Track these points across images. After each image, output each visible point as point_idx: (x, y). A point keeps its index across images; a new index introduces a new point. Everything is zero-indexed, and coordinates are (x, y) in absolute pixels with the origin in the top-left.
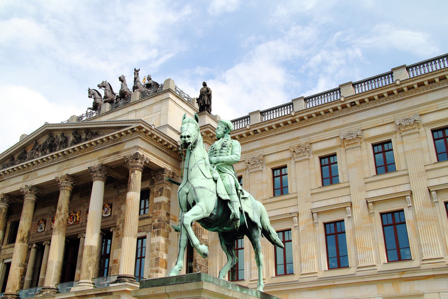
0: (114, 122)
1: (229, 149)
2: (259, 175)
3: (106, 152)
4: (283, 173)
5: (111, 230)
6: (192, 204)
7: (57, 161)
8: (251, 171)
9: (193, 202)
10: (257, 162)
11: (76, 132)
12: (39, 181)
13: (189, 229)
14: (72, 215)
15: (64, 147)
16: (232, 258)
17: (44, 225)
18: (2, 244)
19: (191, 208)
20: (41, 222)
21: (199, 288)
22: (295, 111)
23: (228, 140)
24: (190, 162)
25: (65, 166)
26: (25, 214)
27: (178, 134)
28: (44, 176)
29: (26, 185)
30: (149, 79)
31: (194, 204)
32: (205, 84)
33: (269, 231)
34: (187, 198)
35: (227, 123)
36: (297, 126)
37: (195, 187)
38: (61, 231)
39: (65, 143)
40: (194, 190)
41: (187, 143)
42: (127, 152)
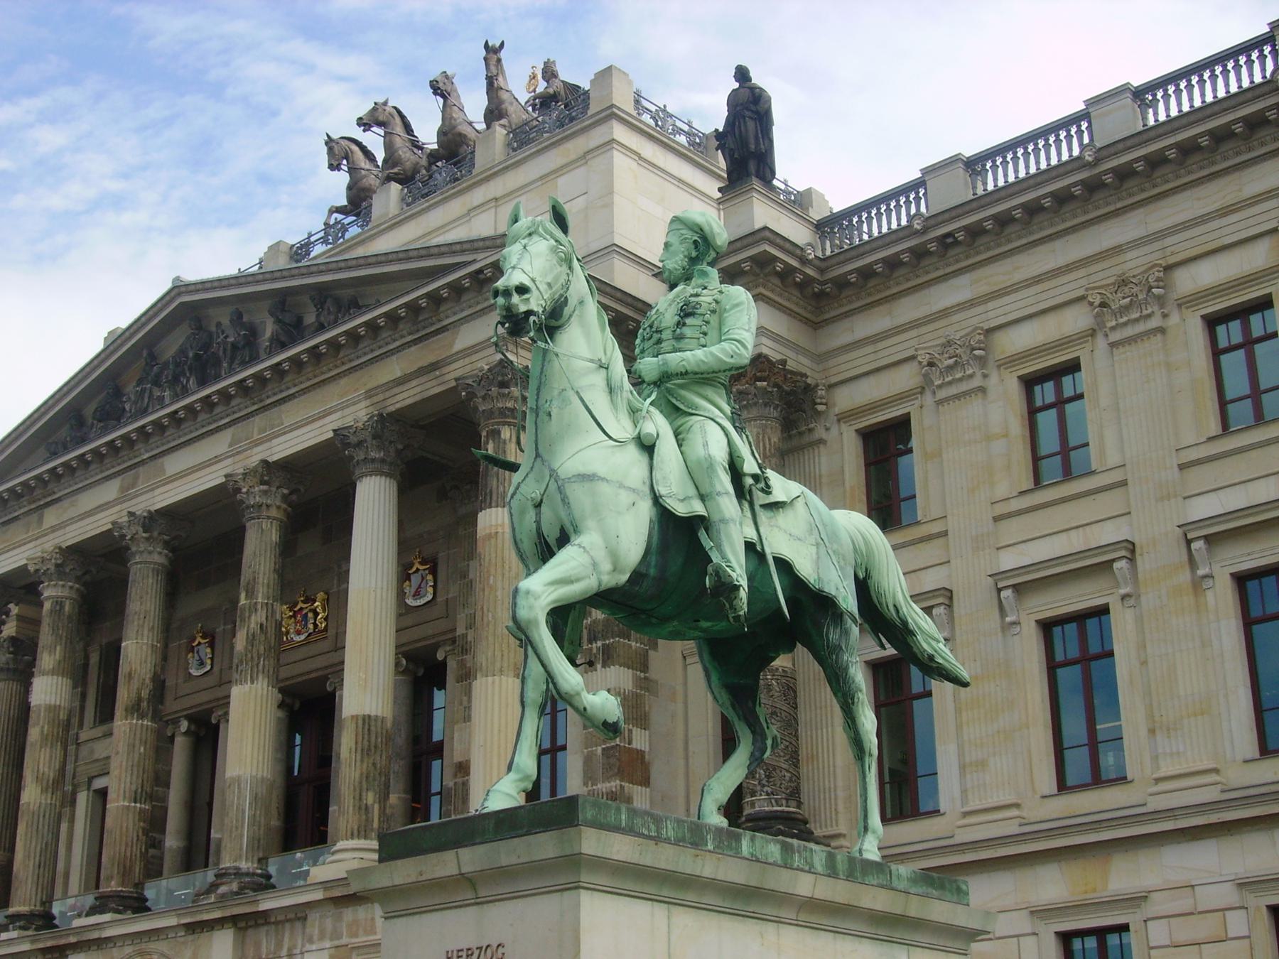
0: (427, 252)
1: (708, 322)
2: (972, 410)
3: (393, 369)
4: (1068, 392)
5: (440, 656)
7: (228, 415)
8: (942, 394)
9: (559, 535)
10: (965, 358)
11: (283, 303)
12: (172, 493)
13: (540, 636)
15: (245, 364)
17: (209, 650)
18: (81, 725)
20: (199, 639)
21: (568, 853)
22: (1098, 145)
23: (705, 288)
25: (256, 430)
26: (136, 617)
27: (653, 275)
28: (190, 473)
29: (129, 512)
30: (549, 73)
31: (564, 540)
32: (742, 74)
33: (905, 623)
34: (538, 522)
36: (1108, 204)
38: (261, 668)
39: (247, 349)
40: (560, 490)
41: (517, 315)
42: (467, 360)
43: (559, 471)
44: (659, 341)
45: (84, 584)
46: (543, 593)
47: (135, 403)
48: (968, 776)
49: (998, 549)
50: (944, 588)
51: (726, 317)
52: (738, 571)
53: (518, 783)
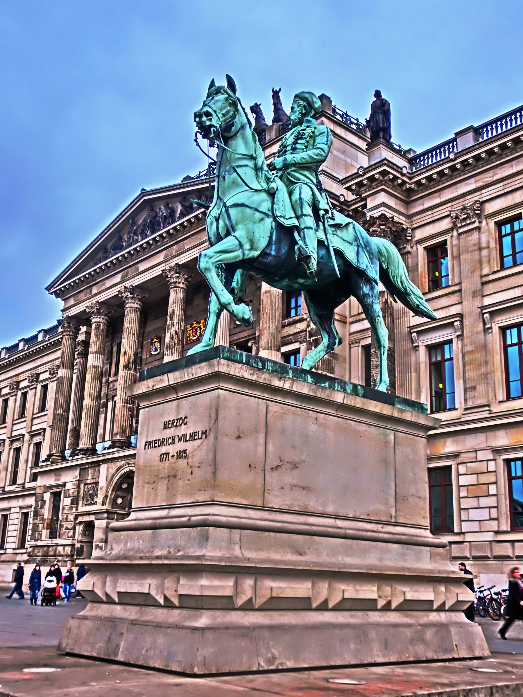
10: (471, 214)
14: (195, 326)
17: (159, 344)
18: (110, 376)
25: (174, 251)
27: (338, 182)
32: (378, 94)
38: (176, 349)
39: (171, 217)
40: (227, 211)
45: (109, 317)
46: (214, 256)
47: (127, 241)
48: (468, 393)
52: (311, 248)
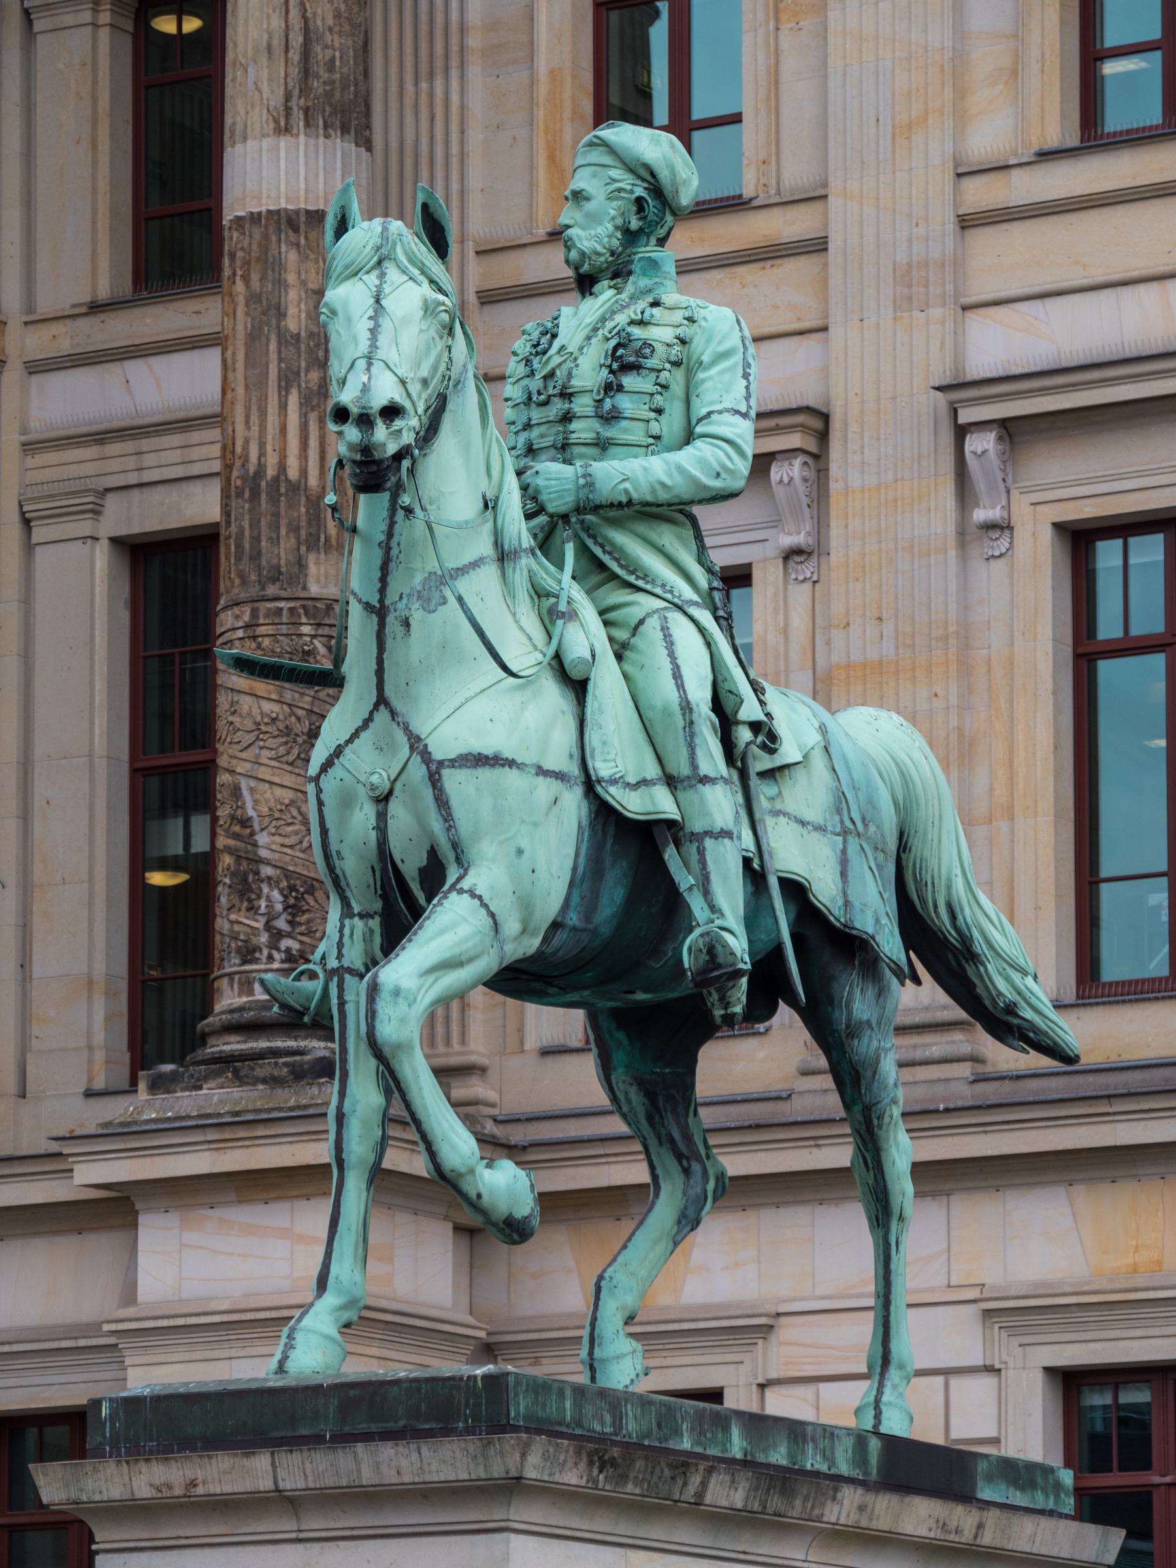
1: (665, 387)
6: (416, 874)
9: (425, 862)
13: (414, 1070)
16: (686, 1171)
19: (417, 913)
24: (392, 565)
33: (966, 941)
35: (647, 167)
37: (438, 755)
40: (434, 780)
43: (429, 741)
44: (567, 418)
46: (419, 990)
49: (965, 308)
50: (808, 410)
51: (703, 381)
53: (338, 1313)
